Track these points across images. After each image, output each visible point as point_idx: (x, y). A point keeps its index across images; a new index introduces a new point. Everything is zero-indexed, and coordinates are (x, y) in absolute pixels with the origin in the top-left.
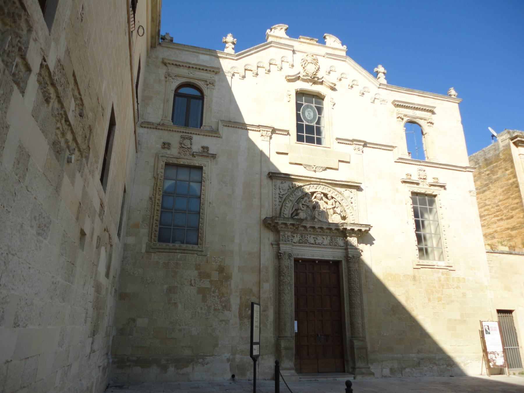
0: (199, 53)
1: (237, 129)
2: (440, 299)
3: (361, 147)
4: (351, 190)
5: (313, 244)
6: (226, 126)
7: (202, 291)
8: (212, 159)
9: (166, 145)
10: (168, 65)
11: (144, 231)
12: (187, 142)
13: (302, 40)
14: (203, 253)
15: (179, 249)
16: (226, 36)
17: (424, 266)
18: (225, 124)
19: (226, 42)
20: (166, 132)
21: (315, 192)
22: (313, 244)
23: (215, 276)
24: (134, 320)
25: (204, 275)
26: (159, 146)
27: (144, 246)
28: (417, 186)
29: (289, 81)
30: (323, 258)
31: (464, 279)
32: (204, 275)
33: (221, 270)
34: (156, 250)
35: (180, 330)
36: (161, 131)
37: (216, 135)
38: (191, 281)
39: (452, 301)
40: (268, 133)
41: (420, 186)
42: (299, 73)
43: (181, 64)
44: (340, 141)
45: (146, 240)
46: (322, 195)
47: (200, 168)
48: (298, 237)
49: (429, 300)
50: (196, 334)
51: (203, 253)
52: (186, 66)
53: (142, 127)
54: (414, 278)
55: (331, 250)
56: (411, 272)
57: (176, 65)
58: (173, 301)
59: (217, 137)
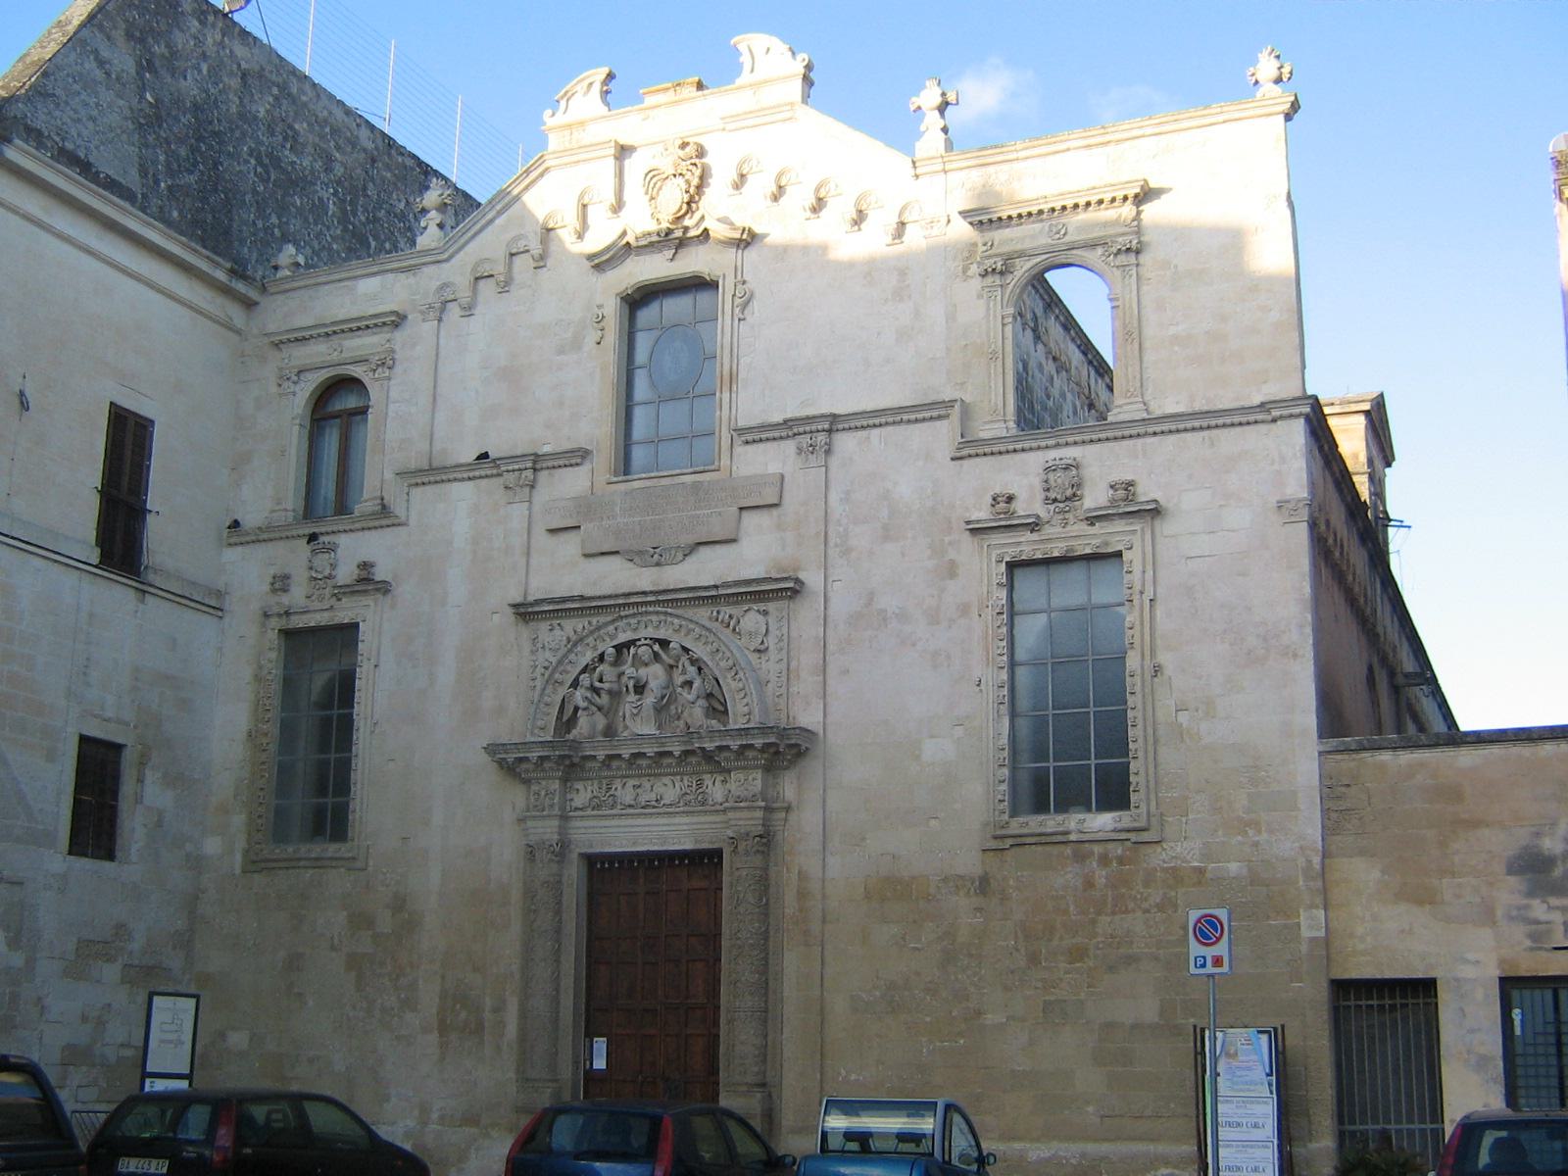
0: (355, 278)
1: (448, 486)
2: (1078, 954)
3: (821, 438)
4: (762, 606)
5: (630, 806)
6: (417, 484)
7: (354, 962)
8: (379, 596)
9: (281, 583)
10: (281, 346)
11: (239, 820)
12: (322, 561)
13: (649, 101)
14: (358, 864)
15: (305, 859)
16: (1255, 62)
17: (1020, 842)
18: (413, 481)
19: (424, 211)
20: (281, 543)
21: (633, 642)
22: (630, 806)
23: (385, 923)
24: (222, 1036)
25: (361, 921)
26: (266, 587)
27: (239, 857)
28: (1035, 536)
29: (598, 268)
30: (664, 848)
31: (1201, 871)
32: (361, 921)
33: (399, 904)
34: (263, 865)
35: (311, 1061)
36: (270, 544)
37: (389, 522)
38: (332, 938)
39: (1131, 960)
40: (524, 473)
41: (1048, 531)
42: (624, 233)
43: (307, 334)
44: (750, 438)
45: (241, 844)
46: (656, 647)
47: (1076, 466)
48: (589, 788)
49: (1034, 959)
50: (343, 1069)
51: (358, 864)
52: (319, 335)
53: (230, 545)
54: (984, 885)
55: (686, 820)
56: (969, 863)
57: (297, 340)
58: (296, 990)
59: (394, 525)
